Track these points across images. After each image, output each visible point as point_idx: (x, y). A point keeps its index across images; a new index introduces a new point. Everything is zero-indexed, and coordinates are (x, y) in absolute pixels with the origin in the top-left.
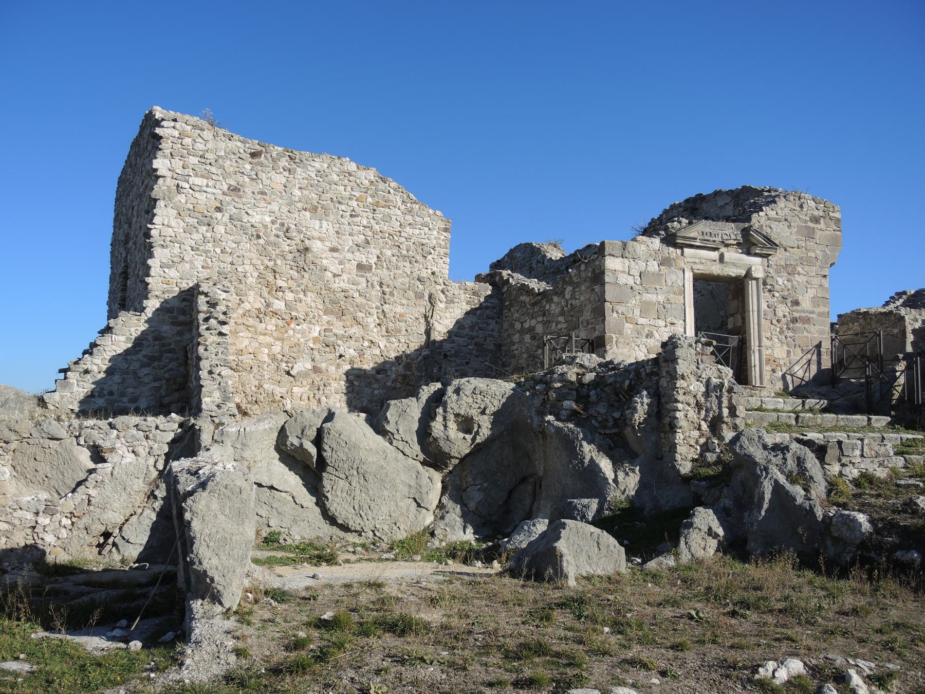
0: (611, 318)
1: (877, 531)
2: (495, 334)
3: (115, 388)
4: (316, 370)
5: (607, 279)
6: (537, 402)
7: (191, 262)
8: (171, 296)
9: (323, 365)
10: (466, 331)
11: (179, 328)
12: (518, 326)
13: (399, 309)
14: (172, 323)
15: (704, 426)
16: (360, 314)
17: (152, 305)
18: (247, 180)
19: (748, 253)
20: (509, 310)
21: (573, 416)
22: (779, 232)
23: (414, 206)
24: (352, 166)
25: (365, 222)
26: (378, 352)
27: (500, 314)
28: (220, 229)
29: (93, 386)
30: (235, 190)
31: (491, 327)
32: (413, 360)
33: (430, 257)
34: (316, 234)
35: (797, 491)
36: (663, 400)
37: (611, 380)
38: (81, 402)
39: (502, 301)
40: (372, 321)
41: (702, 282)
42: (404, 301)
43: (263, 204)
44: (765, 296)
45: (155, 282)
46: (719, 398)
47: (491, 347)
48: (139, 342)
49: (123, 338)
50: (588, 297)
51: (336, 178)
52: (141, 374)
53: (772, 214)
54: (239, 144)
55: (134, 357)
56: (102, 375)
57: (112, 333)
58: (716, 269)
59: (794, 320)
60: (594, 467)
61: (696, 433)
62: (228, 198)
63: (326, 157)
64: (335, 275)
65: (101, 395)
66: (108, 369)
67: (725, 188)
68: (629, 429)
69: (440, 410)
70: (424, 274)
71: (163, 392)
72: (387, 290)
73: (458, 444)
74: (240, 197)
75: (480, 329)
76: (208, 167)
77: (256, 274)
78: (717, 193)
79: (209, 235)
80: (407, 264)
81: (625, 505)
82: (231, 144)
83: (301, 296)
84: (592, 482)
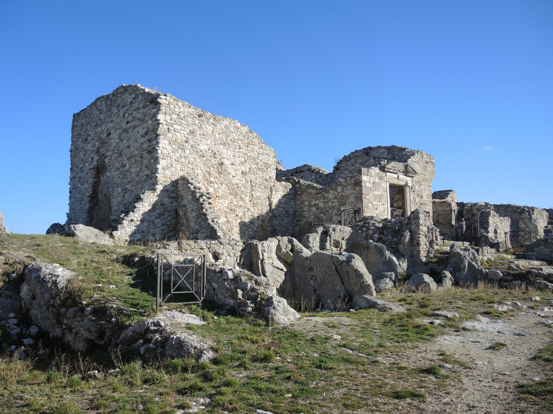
0: (365, 201)
1: (504, 275)
2: (293, 206)
3: (145, 229)
4: (228, 222)
5: (363, 185)
6: (364, 235)
7: (175, 167)
8: (168, 183)
9: (231, 220)
10: (282, 205)
11: (171, 200)
12: (307, 203)
13: (258, 194)
14: (168, 197)
15: (428, 244)
16: (243, 196)
17: (159, 188)
18: (197, 128)
19: (406, 176)
20: (301, 196)
21: (379, 240)
22: (416, 167)
23: (263, 145)
24: (239, 125)
25: (244, 152)
26: (250, 214)
27: (295, 197)
28: (187, 152)
29: (135, 228)
30: (192, 132)
31: (291, 203)
32: (265, 218)
33: (269, 169)
34: (225, 156)
35: (474, 263)
36: (413, 234)
37: (390, 226)
38: (130, 236)
39: (296, 192)
40: (247, 199)
42: (260, 190)
43: (204, 140)
44: (412, 193)
45: (160, 176)
46: (432, 233)
47: (292, 213)
48: (154, 206)
49: (147, 204)
50: (352, 191)
51: (233, 130)
52: (156, 222)
53: (414, 159)
54: (193, 110)
55: (152, 214)
56: (139, 223)
57: (142, 201)
58: (396, 182)
59: (421, 204)
60: (391, 261)
61: (425, 246)
62: (190, 137)
63: (228, 119)
64: (233, 177)
65: (138, 233)
66: (141, 219)
67: (383, 145)
68: (402, 245)
69: (328, 238)
70: (268, 177)
71: (165, 231)
72: (253, 184)
74: (195, 136)
75: (288, 204)
76: (181, 120)
77: (202, 174)
78: (379, 147)
79: (183, 154)
80: (261, 172)
81: (405, 274)
82: (190, 110)
83: (220, 186)
84: (391, 266)
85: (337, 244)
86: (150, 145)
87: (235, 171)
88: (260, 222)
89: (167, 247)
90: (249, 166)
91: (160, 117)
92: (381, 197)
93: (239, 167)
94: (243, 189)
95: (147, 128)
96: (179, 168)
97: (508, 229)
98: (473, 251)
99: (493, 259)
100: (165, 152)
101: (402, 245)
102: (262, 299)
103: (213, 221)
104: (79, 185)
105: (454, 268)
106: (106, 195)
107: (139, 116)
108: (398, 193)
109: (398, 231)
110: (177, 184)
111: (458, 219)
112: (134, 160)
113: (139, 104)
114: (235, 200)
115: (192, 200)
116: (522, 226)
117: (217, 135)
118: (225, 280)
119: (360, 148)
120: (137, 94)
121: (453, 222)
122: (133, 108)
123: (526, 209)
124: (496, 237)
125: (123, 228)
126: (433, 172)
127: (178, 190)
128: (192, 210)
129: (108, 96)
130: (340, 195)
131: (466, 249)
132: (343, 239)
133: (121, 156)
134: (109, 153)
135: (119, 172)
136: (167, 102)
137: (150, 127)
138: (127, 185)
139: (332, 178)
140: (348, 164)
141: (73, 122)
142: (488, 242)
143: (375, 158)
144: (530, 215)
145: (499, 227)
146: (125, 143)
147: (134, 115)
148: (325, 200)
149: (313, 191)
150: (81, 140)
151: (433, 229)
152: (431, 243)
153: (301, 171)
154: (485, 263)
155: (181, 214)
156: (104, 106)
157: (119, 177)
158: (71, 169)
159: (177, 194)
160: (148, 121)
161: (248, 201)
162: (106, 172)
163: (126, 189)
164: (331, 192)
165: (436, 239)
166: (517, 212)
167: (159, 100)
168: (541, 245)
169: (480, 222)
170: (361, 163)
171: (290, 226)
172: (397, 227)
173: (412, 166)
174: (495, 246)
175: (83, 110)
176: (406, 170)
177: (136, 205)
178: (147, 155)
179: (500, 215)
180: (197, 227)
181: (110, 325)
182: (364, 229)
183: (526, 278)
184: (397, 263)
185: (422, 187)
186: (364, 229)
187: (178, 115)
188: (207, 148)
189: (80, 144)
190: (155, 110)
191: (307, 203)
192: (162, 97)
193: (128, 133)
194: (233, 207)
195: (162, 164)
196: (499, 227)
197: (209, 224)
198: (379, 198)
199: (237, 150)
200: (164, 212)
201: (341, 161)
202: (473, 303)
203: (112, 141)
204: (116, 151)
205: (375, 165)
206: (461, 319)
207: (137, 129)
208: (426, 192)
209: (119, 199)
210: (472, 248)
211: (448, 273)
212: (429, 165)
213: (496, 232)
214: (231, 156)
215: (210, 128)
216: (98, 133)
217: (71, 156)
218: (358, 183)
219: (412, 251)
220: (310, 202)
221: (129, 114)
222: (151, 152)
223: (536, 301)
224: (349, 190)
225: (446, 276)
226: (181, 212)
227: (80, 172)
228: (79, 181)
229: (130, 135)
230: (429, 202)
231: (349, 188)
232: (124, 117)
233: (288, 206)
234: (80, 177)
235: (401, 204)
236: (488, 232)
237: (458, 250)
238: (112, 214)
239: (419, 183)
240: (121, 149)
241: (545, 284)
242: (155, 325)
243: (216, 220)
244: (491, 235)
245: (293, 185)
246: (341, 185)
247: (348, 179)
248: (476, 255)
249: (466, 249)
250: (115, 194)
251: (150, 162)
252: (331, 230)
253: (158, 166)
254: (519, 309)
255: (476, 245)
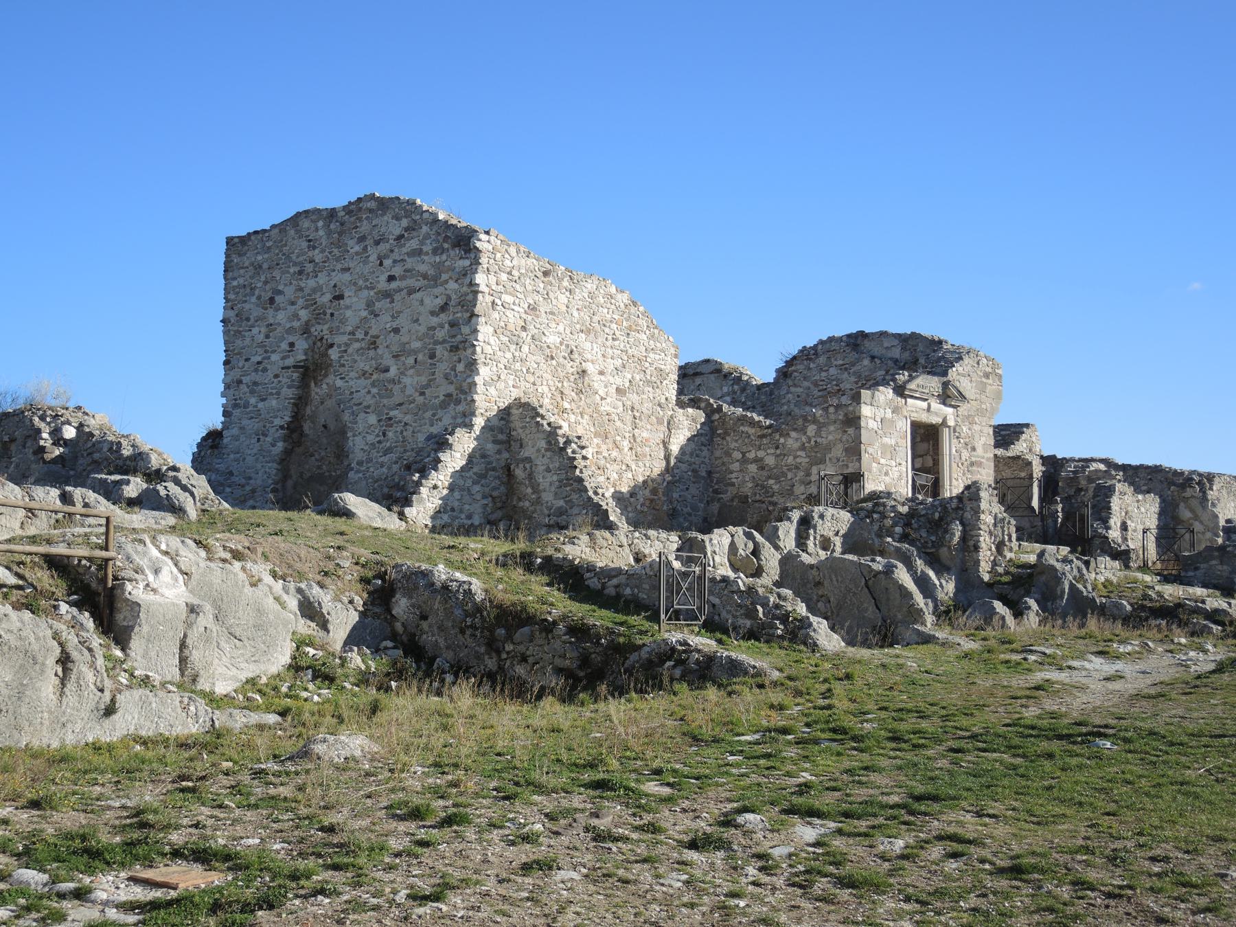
0: (865, 457)
2: (707, 460)
3: (456, 504)
5: (863, 424)
6: (876, 527)
7: (506, 382)
10: (687, 458)
12: (737, 455)
13: (645, 435)
16: (618, 438)
17: (479, 422)
19: (944, 404)
21: (904, 538)
22: (966, 386)
26: (630, 475)
27: (711, 442)
28: (525, 348)
34: (589, 356)
35: (1080, 586)
38: (433, 518)
39: (713, 431)
40: (626, 444)
41: (916, 427)
42: (649, 427)
43: (554, 325)
44: (954, 441)
46: (1002, 528)
49: (458, 455)
53: (960, 369)
56: (445, 492)
58: (924, 418)
59: (972, 464)
62: (530, 318)
64: (602, 399)
66: (450, 484)
67: (893, 330)
68: (945, 549)
69: (811, 531)
72: (637, 414)
73: (588, 575)
78: (883, 334)
79: (517, 354)
85: (826, 544)
86: (453, 333)
87: (606, 387)
88: (647, 492)
89: (576, 541)
90: (629, 376)
91: (480, 278)
92: (894, 449)
93: (612, 380)
94: (618, 423)
95: (444, 297)
96: (511, 383)
97: (1152, 523)
98: (1079, 563)
99: (1115, 580)
100: (488, 350)
101: (945, 549)
102: (795, 619)
103: (596, 493)
104: (253, 401)
105: (1043, 594)
106: (325, 426)
107: (423, 268)
108: (926, 439)
109: (933, 524)
110: (509, 414)
111: (1046, 499)
112: (411, 361)
113: (422, 243)
114: (604, 447)
115: (547, 450)
116: (1185, 514)
117: (575, 314)
118: (733, 592)
119: (840, 332)
120: (415, 221)
121: (1035, 503)
122: (404, 250)
123: (1196, 478)
124: (1125, 539)
125: (421, 501)
126: (998, 396)
127: (514, 425)
128: (548, 470)
129: (332, 213)
130: (813, 443)
131: (1065, 560)
132: (837, 534)
133: (375, 349)
134: (341, 339)
135: (369, 381)
136: (490, 248)
137: (454, 297)
138: (392, 409)
139: (771, 393)
140: (812, 365)
141: (227, 255)
142: (1107, 547)
143: (873, 358)
144: (1204, 493)
145: (1134, 517)
146: (385, 321)
147: (408, 266)
148: (778, 452)
149: (751, 431)
150: (254, 299)
151: (1003, 519)
152: (1000, 546)
153: (696, 374)
154: (1101, 587)
155: (523, 479)
156: (321, 233)
157: (369, 392)
158: (226, 363)
159: (509, 435)
160: (446, 282)
161: (626, 449)
162: (326, 376)
163: (390, 419)
164: (793, 434)
165: (1010, 540)
166: (1174, 484)
167: (478, 244)
168: (1213, 558)
169: (1093, 507)
170: (840, 367)
171: (701, 501)
172: (937, 515)
173: (957, 384)
174: (1123, 556)
175: (256, 232)
176: (944, 392)
177: (442, 456)
178: (446, 353)
179: (1138, 490)
180: (561, 503)
181: (599, 649)
182: (875, 516)
183: (1172, 613)
184: (937, 582)
185: (977, 427)
186: (875, 516)
187: (510, 273)
188: (558, 340)
189: (252, 307)
190: (467, 263)
191: (737, 455)
192: (483, 237)
193: (392, 302)
194: (602, 462)
195: (484, 373)
196: (1134, 517)
197: (590, 498)
198: (892, 451)
199: (609, 343)
200: (487, 470)
201: (794, 358)
202: (1080, 641)
203: (349, 313)
204: (360, 335)
205: (885, 383)
206: (1064, 657)
207: (418, 295)
208: (983, 439)
209: (371, 438)
210: (1078, 558)
211: (1032, 602)
212: (990, 381)
213: (1124, 527)
214: (600, 355)
215: (563, 299)
216: (307, 291)
217: (226, 333)
218: (853, 421)
219: (963, 562)
220: (744, 454)
221: (395, 261)
222: (460, 346)
223: (1180, 644)
224: (832, 434)
225: (1029, 608)
226: (519, 473)
227: (256, 370)
228: (252, 392)
229: (397, 306)
230: (988, 459)
231: (832, 428)
232: (381, 264)
233: (698, 461)
234: (255, 384)
235: (930, 463)
236: (1108, 528)
237: (1053, 562)
238: (352, 469)
239: (970, 419)
240: (373, 332)
241: (1205, 626)
242: (681, 645)
243: (600, 491)
244: (1114, 534)
245: (708, 416)
246: (815, 421)
247: (831, 410)
248: (1085, 571)
249: (1065, 560)
250: (360, 426)
251: (454, 369)
252: (816, 516)
253: (477, 379)
254: (1150, 651)
255: (1083, 553)
